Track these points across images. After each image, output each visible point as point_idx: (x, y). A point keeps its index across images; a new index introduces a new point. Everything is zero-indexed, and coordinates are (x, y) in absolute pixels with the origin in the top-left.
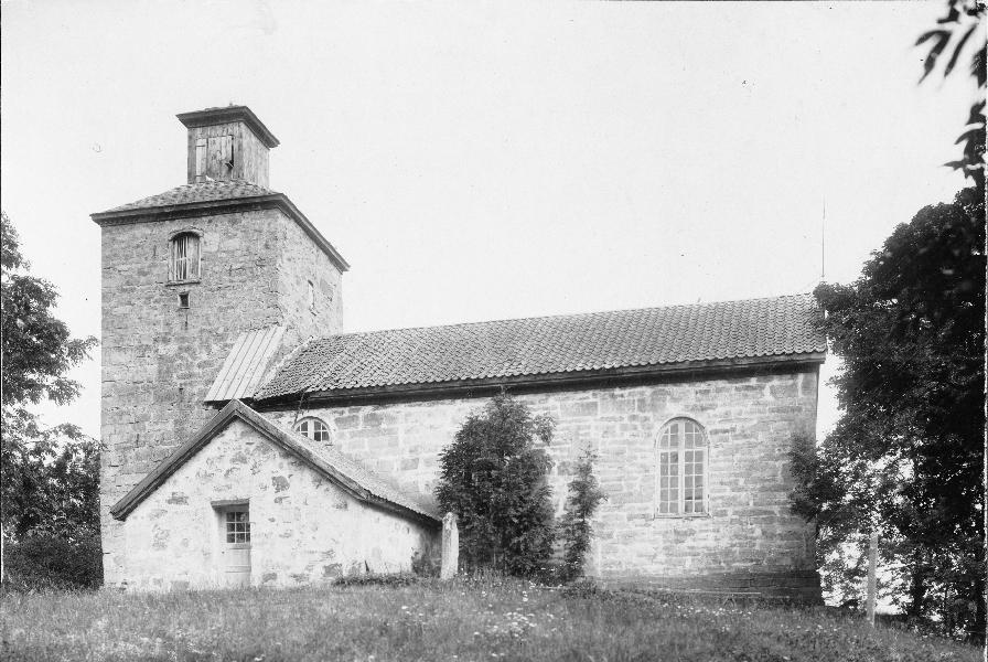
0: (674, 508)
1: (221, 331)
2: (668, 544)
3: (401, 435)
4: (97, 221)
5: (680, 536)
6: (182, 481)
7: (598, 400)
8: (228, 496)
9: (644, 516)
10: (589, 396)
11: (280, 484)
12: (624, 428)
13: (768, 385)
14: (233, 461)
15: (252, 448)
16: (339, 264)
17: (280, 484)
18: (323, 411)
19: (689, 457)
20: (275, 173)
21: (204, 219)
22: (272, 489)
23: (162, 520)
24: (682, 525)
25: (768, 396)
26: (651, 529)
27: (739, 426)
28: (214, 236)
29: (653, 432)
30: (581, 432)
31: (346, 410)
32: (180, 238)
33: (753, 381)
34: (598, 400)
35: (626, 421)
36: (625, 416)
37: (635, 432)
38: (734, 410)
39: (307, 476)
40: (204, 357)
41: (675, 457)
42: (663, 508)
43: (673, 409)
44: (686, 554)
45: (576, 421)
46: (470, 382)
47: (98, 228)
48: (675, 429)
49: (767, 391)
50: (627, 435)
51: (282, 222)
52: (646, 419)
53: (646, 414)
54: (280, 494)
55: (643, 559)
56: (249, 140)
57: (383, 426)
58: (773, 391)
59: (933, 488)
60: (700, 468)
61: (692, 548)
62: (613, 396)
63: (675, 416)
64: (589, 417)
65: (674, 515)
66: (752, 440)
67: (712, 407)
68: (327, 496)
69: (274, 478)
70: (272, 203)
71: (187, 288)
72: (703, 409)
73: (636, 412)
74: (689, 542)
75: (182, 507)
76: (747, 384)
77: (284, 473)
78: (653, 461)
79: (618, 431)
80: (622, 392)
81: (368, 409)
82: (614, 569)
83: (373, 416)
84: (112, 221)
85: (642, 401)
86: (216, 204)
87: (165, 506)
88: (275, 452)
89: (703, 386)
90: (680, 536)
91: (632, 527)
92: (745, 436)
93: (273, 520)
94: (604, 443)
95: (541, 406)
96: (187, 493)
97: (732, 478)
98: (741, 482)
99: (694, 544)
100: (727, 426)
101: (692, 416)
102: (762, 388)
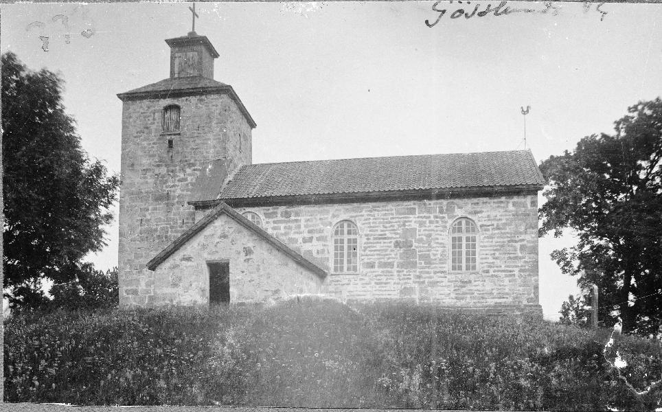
0: (460, 268)
1: (192, 161)
2: (456, 288)
3: (303, 223)
4: (120, 98)
5: (465, 283)
6: (190, 249)
7: (416, 207)
8: (215, 258)
9: (442, 272)
10: (411, 204)
11: (248, 252)
12: (430, 222)
13: (511, 201)
14: (221, 237)
15: (231, 230)
16: (252, 125)
17: (248, 252)
18: (256, 208)
19: (468, 239)
20: (221, 73)
21: (183, 98)
22: (243, 254)
23: (176, 270)
24: (400, 269)
25: (511, 207)
26: (447, 279)
27: (495, 223)
28: (189, 105)
29: (448, 225)
30: (407, 224)
31: (271, 208)
32: (167, 108)
33: (503, 199)
34: (416, 207)
35: (432, 219)
36: (432, 216)
37: (438, 225)
38: (493, 214)
39: (265, 245)
40: (182, 176)
41: (460, 239)
42: (454, 268)
43: (459, 213)
44: (467, 293)
45: (403, 218)
46: (344, 194)
47: (120, 102)
48: (460, 223)
49: (510, 205)
50: (433, 226)
51: (225, 98)
52: (444, 217)
53: (444, 215)
54: (248, 257)
55: (443, 296)
56: (205, 54)
57: (293, 218)
58: (514, 205)
59: (47, 169)
60: (474, 246)
61: (470, 290)
62: (425, 204)
63: (460, 216)
64: (411, 216)
65: (474, 271)
66: (503, 231)
67: (481, 212)
68: (275, 259)
69: (244, 248)
70: (226, 90)
71: (173, 137)
72: (476, 213)
73: (438, 214)
74: (469, 287)
75: (189, 263)
76: (499, 200)
77: (250, 245)
78: (448, 242)
79: (428, 224)
80: (430, 202)
81: (282, 209)
82: (426, 301)
83: (286, 213)
84: (129, 98)
85: (441, 208)
86: (187, 88)
87: (178, 262)
88: (245, 232)
89: (475, 200)
90: (465, 283)
91: (436, 278)
92: (499, 229)
93: (243, 272)
94: (419, 231)
95: (384, 209)
96: (192, 256)
97: (492, 252)
98: (497, 254)
99: (471, 288)
100: (489, 223)
101: (469, 217)
102: (508, 202)
